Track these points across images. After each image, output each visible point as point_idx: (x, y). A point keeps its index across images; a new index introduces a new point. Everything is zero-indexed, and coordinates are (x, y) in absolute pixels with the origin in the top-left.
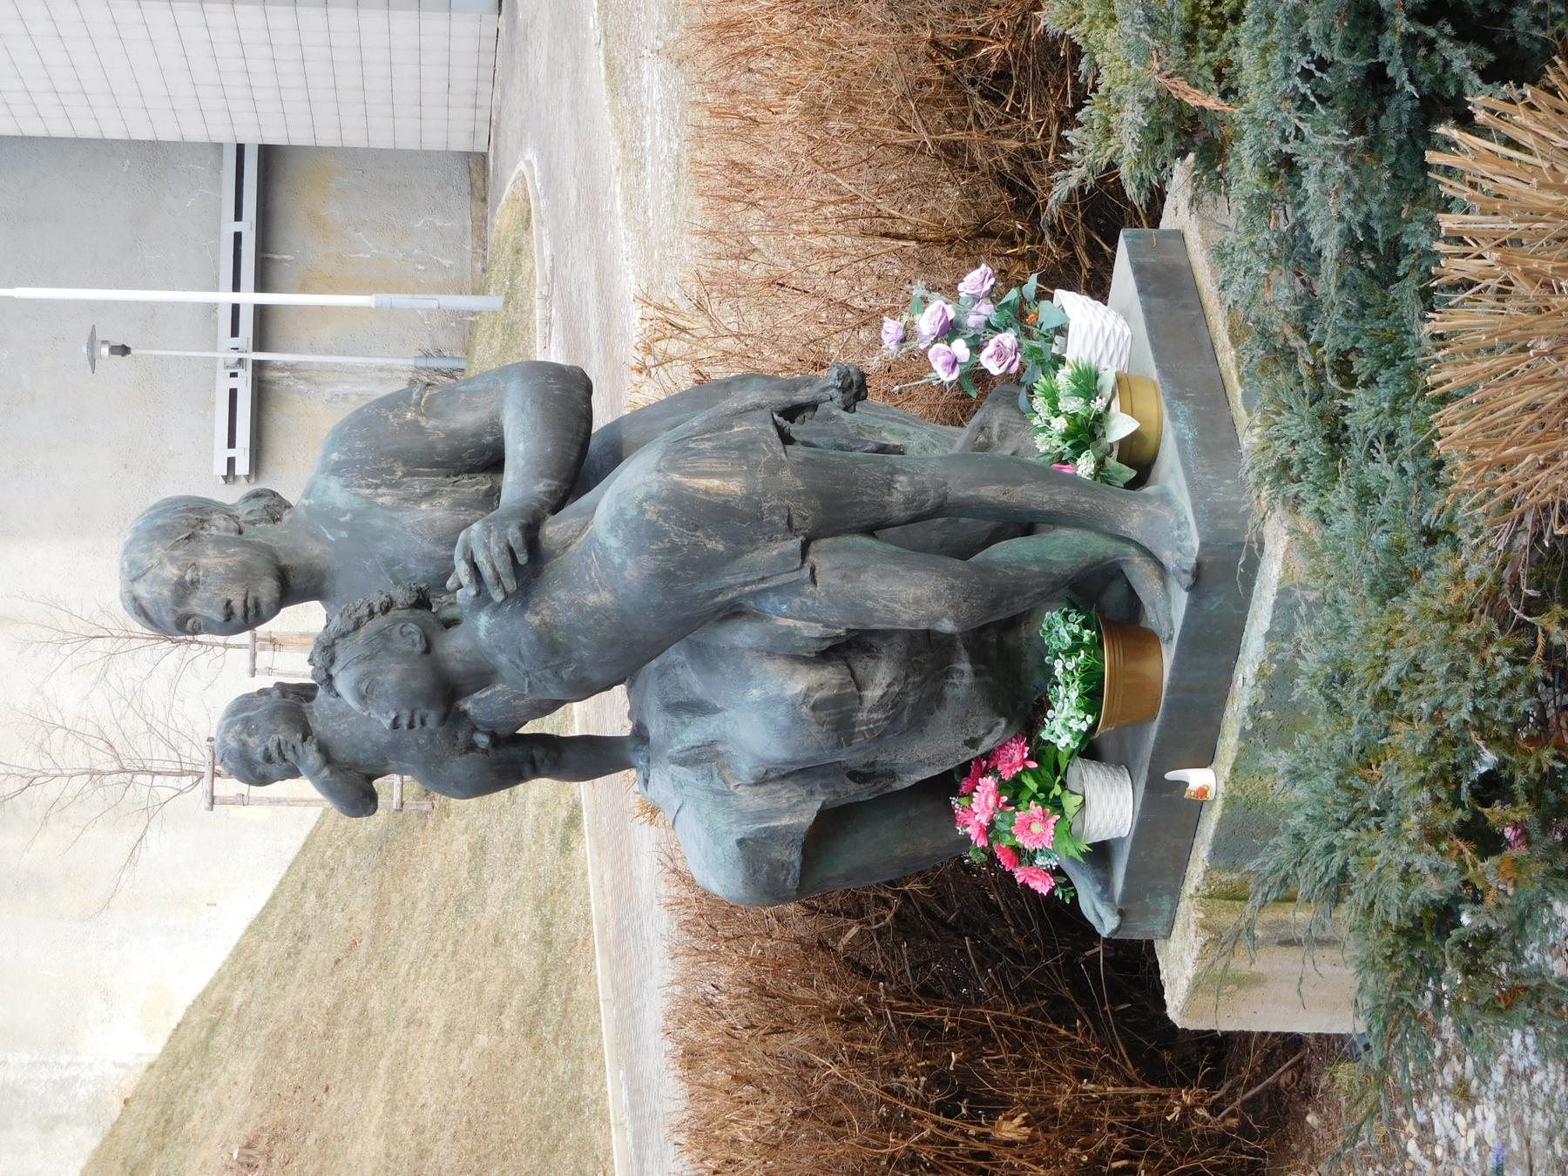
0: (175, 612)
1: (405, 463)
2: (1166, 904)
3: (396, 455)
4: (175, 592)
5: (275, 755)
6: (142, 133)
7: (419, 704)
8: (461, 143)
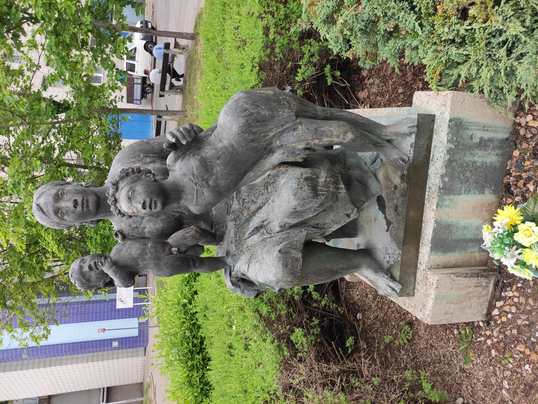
0: (54, 205)
1: (144, 153)
2: (412, 279)
3: (141, 151)
4: (54, 198)
5: (93, 266)
6: (87, 389)
7: (154, 196)
8: (139, 381)
